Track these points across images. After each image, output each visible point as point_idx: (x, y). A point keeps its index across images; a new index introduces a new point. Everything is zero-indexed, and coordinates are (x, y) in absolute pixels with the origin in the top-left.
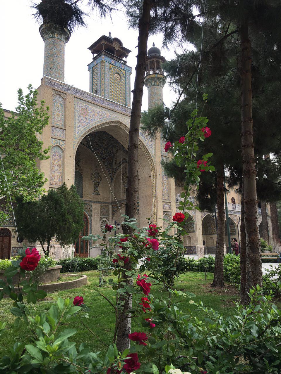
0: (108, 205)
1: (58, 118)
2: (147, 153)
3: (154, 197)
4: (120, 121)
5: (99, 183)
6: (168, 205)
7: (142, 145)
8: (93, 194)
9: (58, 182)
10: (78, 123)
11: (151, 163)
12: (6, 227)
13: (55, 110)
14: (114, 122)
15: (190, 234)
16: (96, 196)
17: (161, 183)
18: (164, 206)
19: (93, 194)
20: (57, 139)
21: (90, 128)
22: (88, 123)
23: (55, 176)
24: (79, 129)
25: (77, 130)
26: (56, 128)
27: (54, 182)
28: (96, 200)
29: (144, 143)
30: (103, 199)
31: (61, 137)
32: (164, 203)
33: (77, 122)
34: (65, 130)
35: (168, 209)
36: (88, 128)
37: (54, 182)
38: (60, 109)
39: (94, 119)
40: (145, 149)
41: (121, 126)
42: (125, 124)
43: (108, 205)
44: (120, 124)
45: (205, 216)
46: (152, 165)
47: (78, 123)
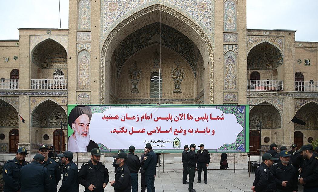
0: (192, 102)
1: (84, 22)
2: (202, 34)
3: (212, 87)
4: (159, 3)
5: (181, 80)
6: (234, 95)
7: (194, 26)
8: (174, 92)
9: (86, 85)
10: (105, 21)
11: (209, 46)
12: (16, 128)
13: (82, 15)
14: (153, 8)
15: (277, 129)
16: (177, 94)
17: (222, 69)
18: (225, 97)
19: (174, 92)
20: (83, 43)
21: (119, 23)
22: (117, 18)
23: (83, 80)
24: (106, 27)
25: (104, 29)
26: (82, 32)
27: (82, 86)
28: (177, 98)
29: (196, 22)
30: (186, 97)
31: (88, 40)
32: (226, 94)
33: (104, 20)
34: (90, 32)
35: (233, 101)
36: (117, 22)
37: (82, 86)
38: (87, 12)
39: (124, 11)
40: (198, 30)
41: (163, 10)
42: (167, 6)
43: (192, 102)
44: (161, 7)
45: (303, 105)
46: (210, 48)
47: (105, 21)
